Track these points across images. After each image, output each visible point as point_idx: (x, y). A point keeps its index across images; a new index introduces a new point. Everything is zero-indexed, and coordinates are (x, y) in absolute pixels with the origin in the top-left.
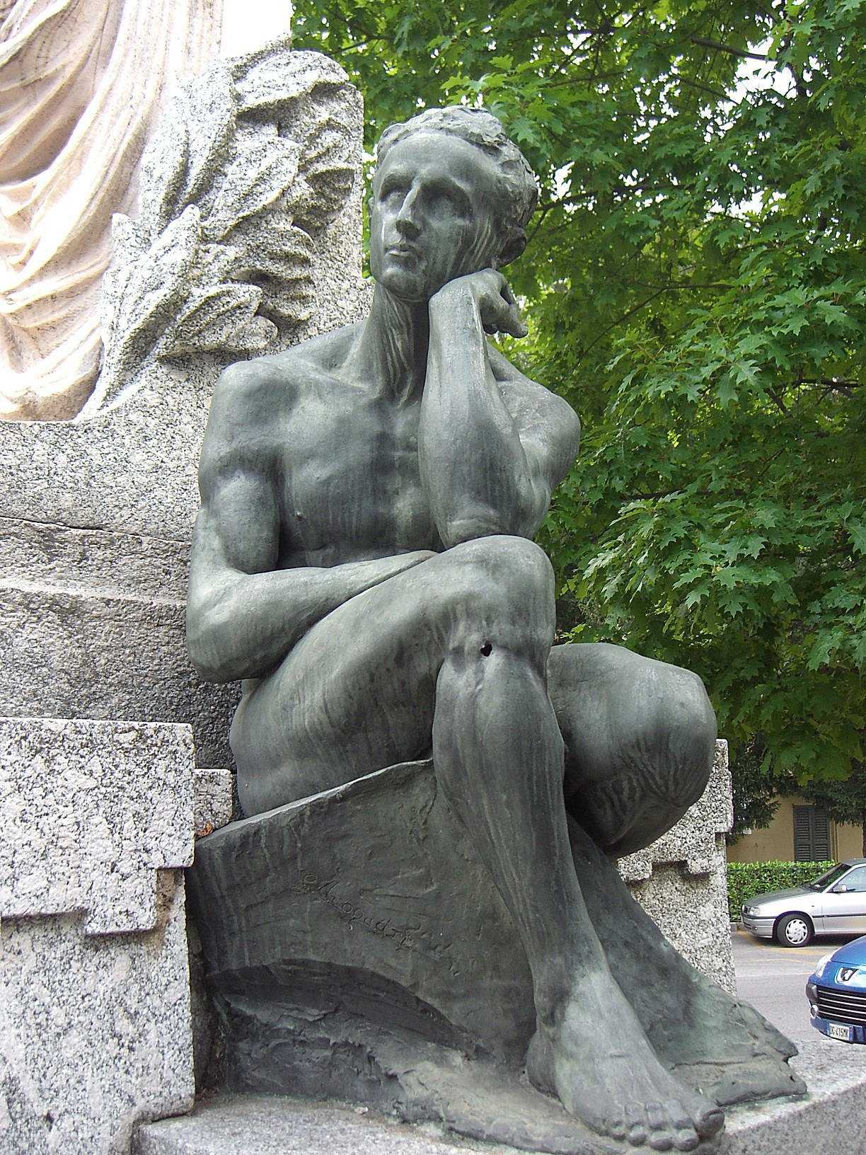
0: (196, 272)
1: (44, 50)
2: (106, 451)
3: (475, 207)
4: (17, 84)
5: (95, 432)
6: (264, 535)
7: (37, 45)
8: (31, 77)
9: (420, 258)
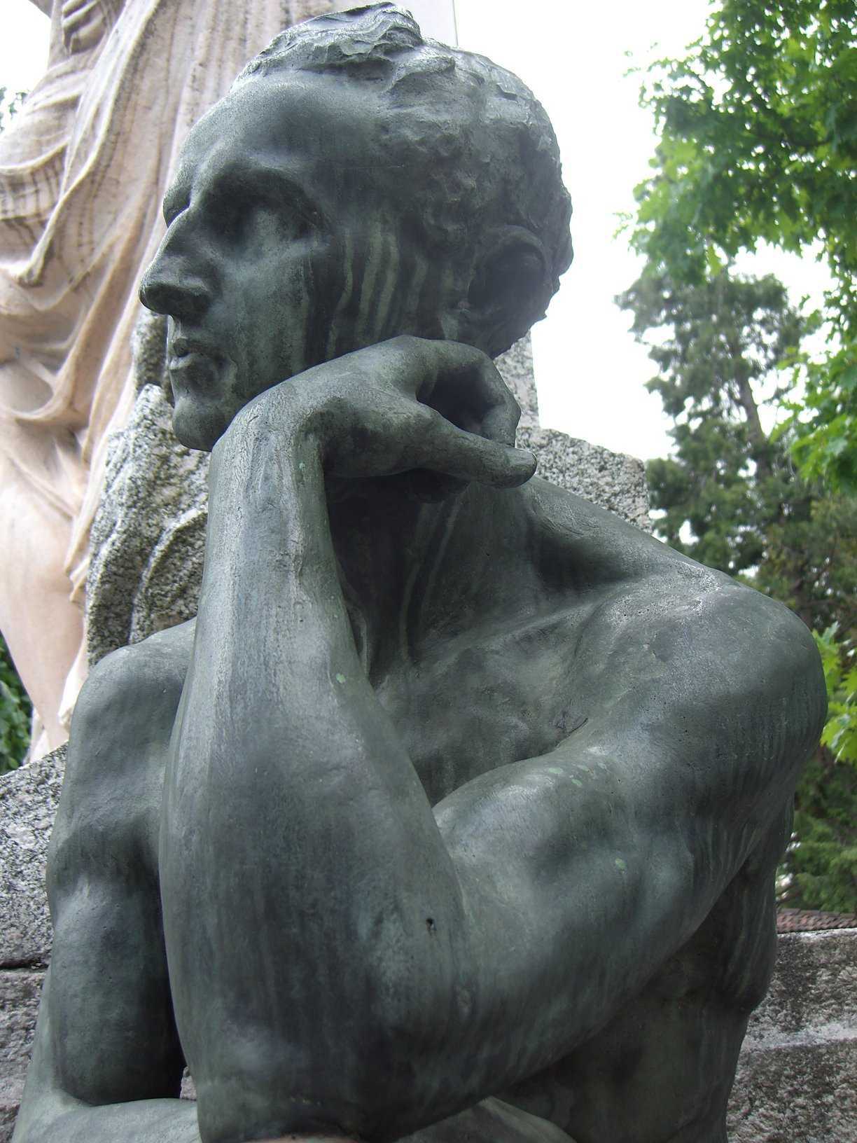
0: (169, 492)
1: (85, 233)
2: (42, 824)
3: (326, 205)
4: (66, 289)
5: (21, 795)
6: (114, 1015)
7: (72, 230)
8: (79, 274)
9: (220, 362)
